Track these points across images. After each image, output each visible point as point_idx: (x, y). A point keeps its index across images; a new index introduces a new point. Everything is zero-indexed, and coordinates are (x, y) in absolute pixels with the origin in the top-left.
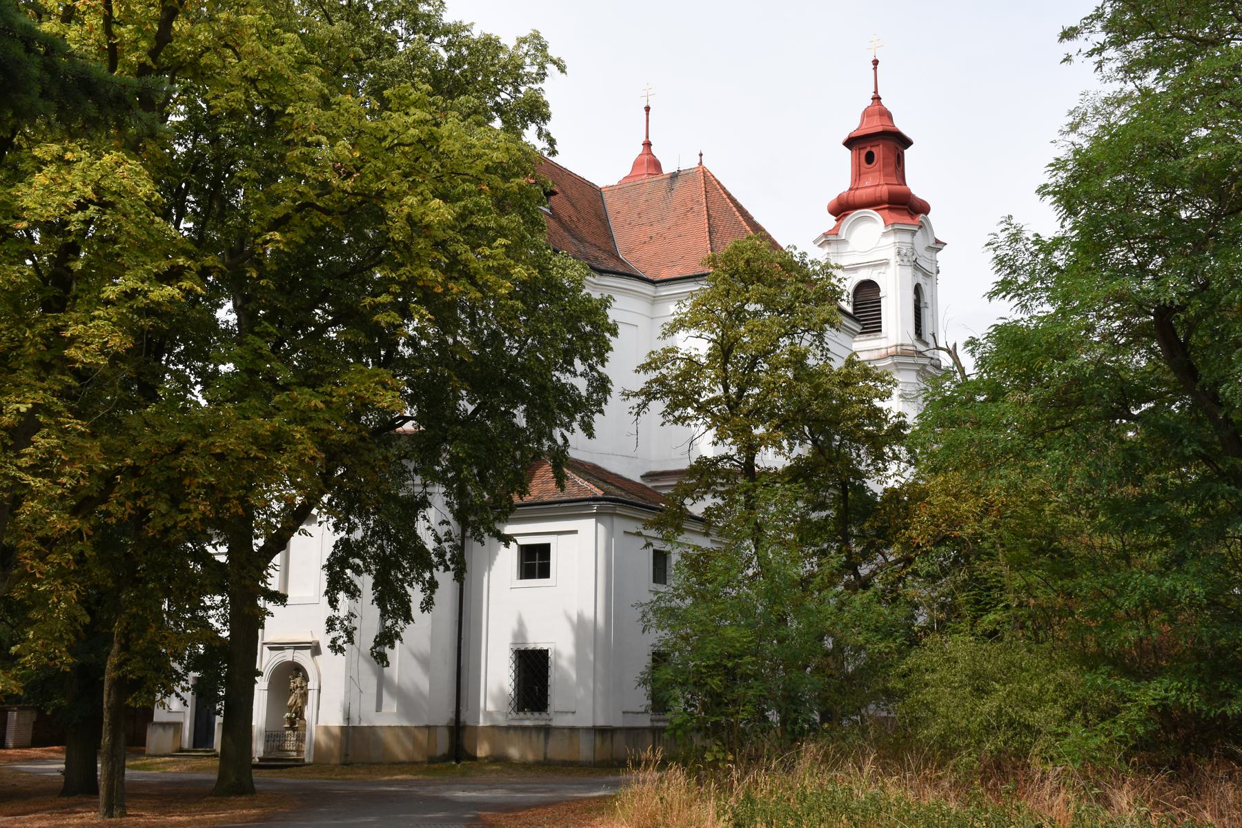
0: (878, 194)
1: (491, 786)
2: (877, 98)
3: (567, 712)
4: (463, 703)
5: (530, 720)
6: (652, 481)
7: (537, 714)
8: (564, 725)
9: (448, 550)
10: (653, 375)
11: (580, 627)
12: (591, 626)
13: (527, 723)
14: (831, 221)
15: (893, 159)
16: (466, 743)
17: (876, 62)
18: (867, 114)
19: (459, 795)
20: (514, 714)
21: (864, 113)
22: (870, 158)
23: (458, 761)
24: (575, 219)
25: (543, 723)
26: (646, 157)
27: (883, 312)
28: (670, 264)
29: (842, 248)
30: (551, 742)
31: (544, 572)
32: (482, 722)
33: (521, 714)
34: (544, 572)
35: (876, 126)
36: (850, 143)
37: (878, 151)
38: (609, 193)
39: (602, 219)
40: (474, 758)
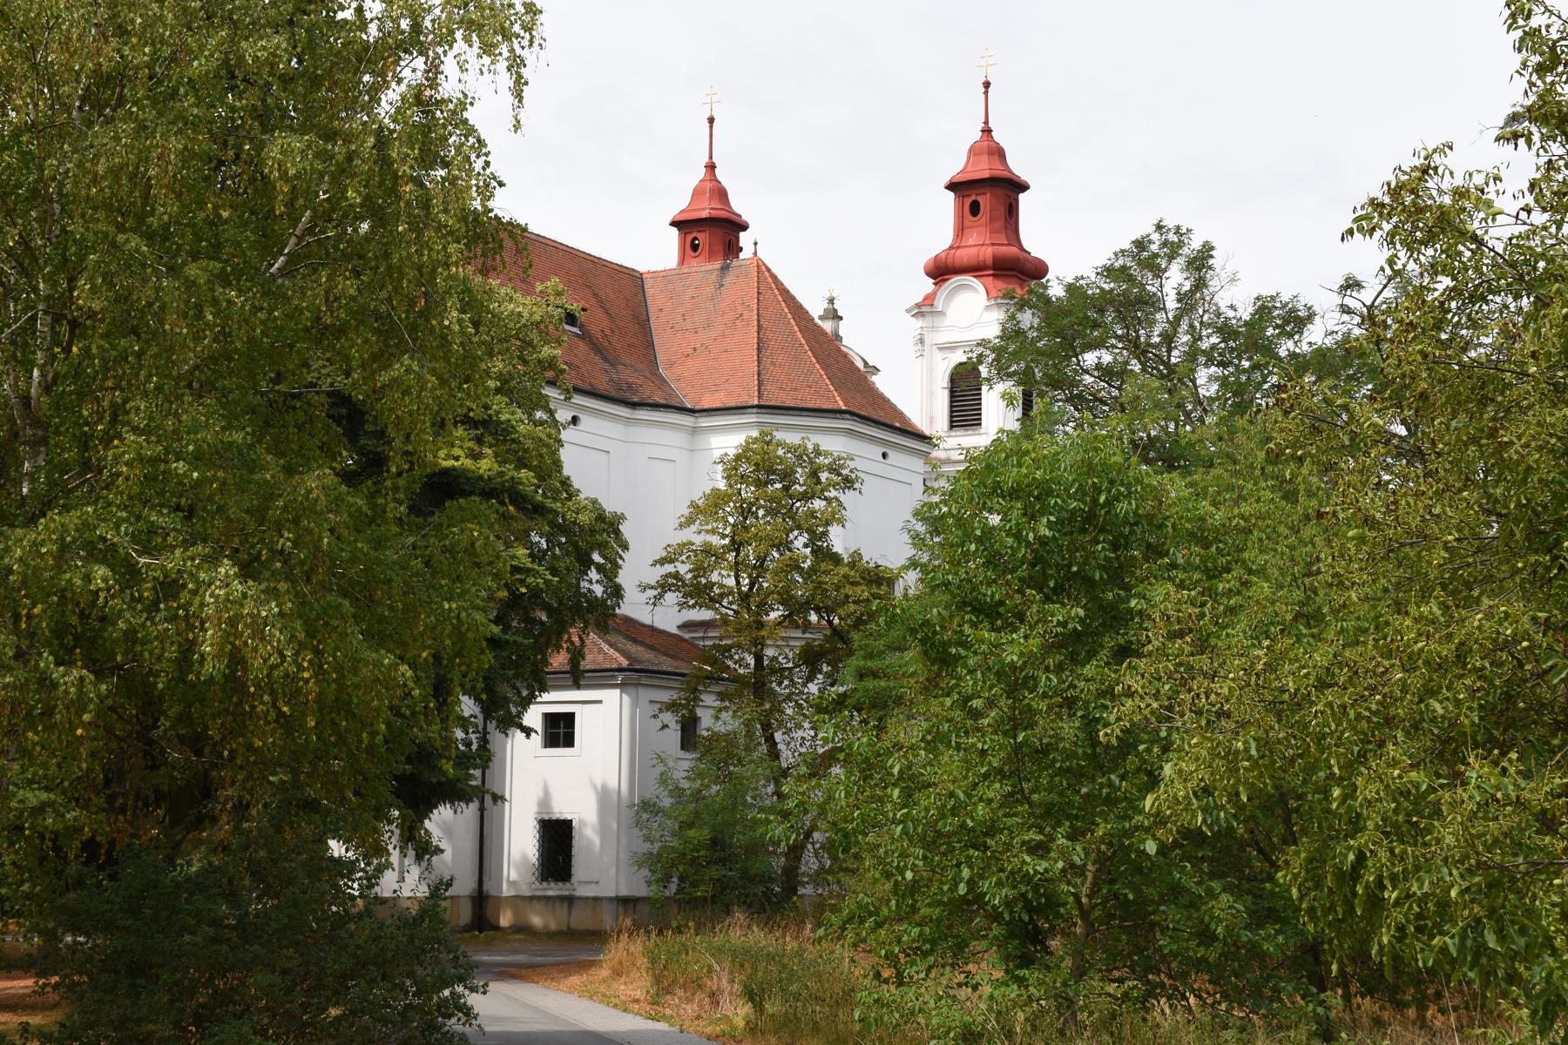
0: (981, 258)
1: (514, 952)
2: (987, 131)
3: (591, 882)
4: (486, 872)
5: (553, 889)
6: (689, 632)
7: (560, 884)
8: (587, 894)
9: (475, 741)
10: (669, 568)
11: (603, 795)
12: (615, 797)
13: (550, 893)
14: (929, 284)
15: (1002, 211)
16: (489, 913)
17: (987, 85)
18: (974, 151)
19: (486, 958)
20: (538, 884)
21: (970, 151)
22: (975, 209)
23: (481, 931)
24: (608, 332)
25: (566, 893)
26: (709, 185)
27: (983, 407)
28: (713, 388)
29: (938, 321)
30: (574, 912)
31: (569, 742)
32: (506, 891)
33: (545, 884)
34: (569, 742)
35: (983, 170)
36: (952, 186)
37: (985, 201)
38: (652, 281)
39: (642, 322)
40: (497, 928)
